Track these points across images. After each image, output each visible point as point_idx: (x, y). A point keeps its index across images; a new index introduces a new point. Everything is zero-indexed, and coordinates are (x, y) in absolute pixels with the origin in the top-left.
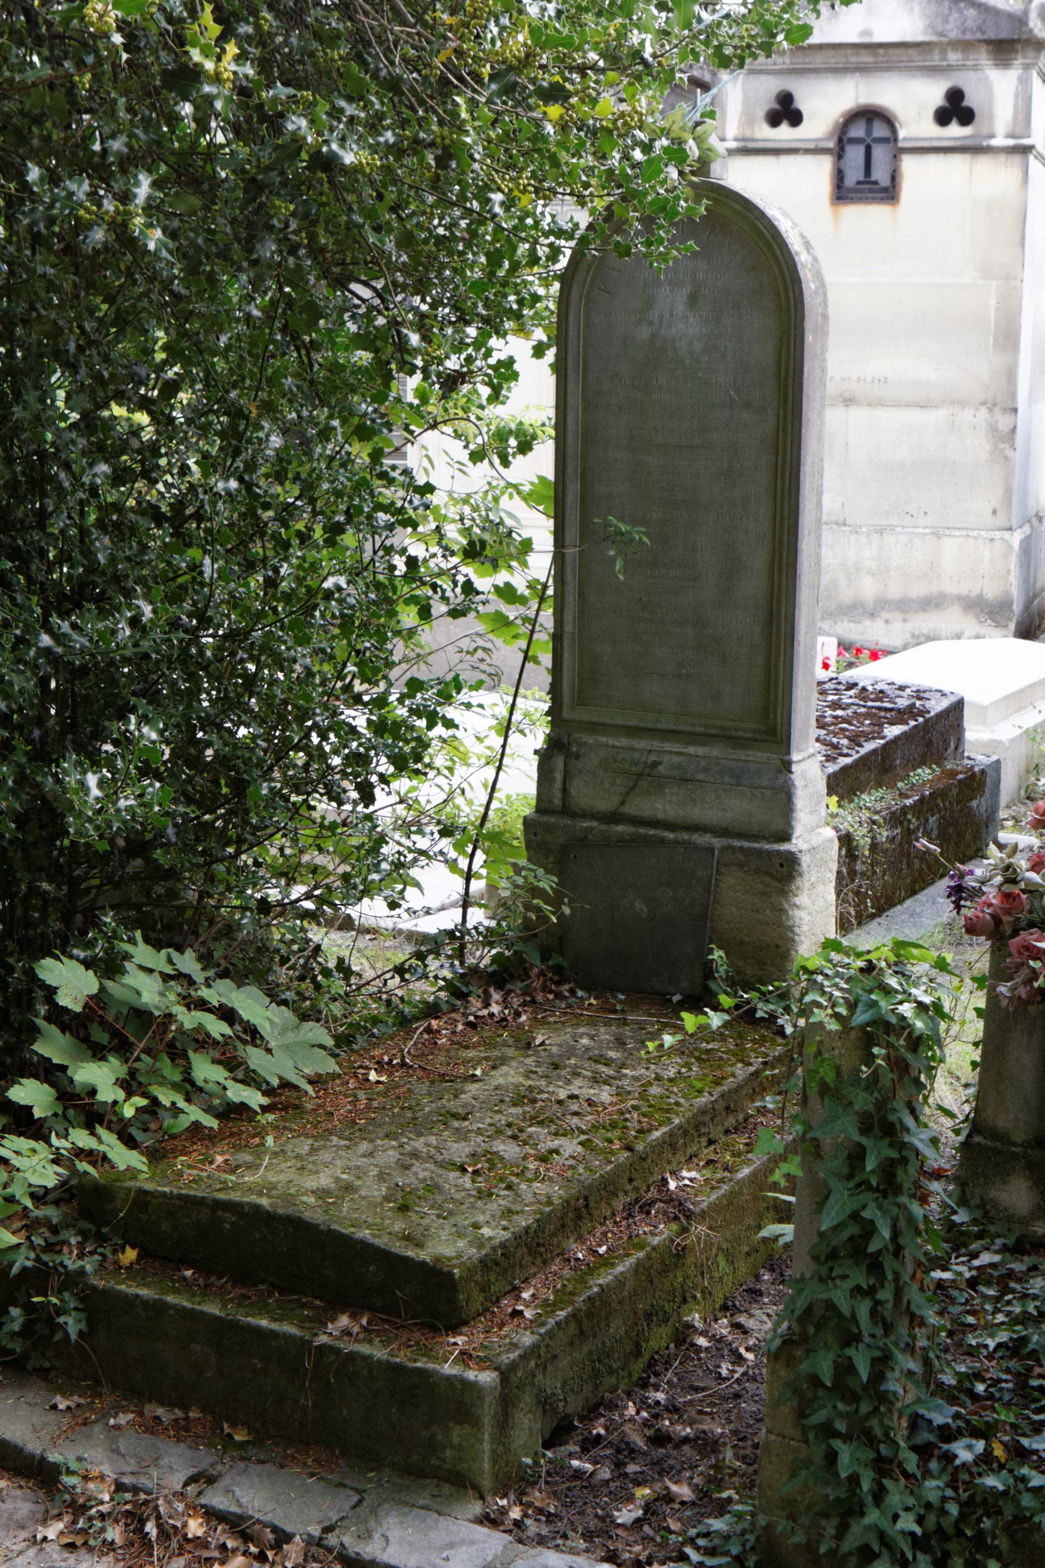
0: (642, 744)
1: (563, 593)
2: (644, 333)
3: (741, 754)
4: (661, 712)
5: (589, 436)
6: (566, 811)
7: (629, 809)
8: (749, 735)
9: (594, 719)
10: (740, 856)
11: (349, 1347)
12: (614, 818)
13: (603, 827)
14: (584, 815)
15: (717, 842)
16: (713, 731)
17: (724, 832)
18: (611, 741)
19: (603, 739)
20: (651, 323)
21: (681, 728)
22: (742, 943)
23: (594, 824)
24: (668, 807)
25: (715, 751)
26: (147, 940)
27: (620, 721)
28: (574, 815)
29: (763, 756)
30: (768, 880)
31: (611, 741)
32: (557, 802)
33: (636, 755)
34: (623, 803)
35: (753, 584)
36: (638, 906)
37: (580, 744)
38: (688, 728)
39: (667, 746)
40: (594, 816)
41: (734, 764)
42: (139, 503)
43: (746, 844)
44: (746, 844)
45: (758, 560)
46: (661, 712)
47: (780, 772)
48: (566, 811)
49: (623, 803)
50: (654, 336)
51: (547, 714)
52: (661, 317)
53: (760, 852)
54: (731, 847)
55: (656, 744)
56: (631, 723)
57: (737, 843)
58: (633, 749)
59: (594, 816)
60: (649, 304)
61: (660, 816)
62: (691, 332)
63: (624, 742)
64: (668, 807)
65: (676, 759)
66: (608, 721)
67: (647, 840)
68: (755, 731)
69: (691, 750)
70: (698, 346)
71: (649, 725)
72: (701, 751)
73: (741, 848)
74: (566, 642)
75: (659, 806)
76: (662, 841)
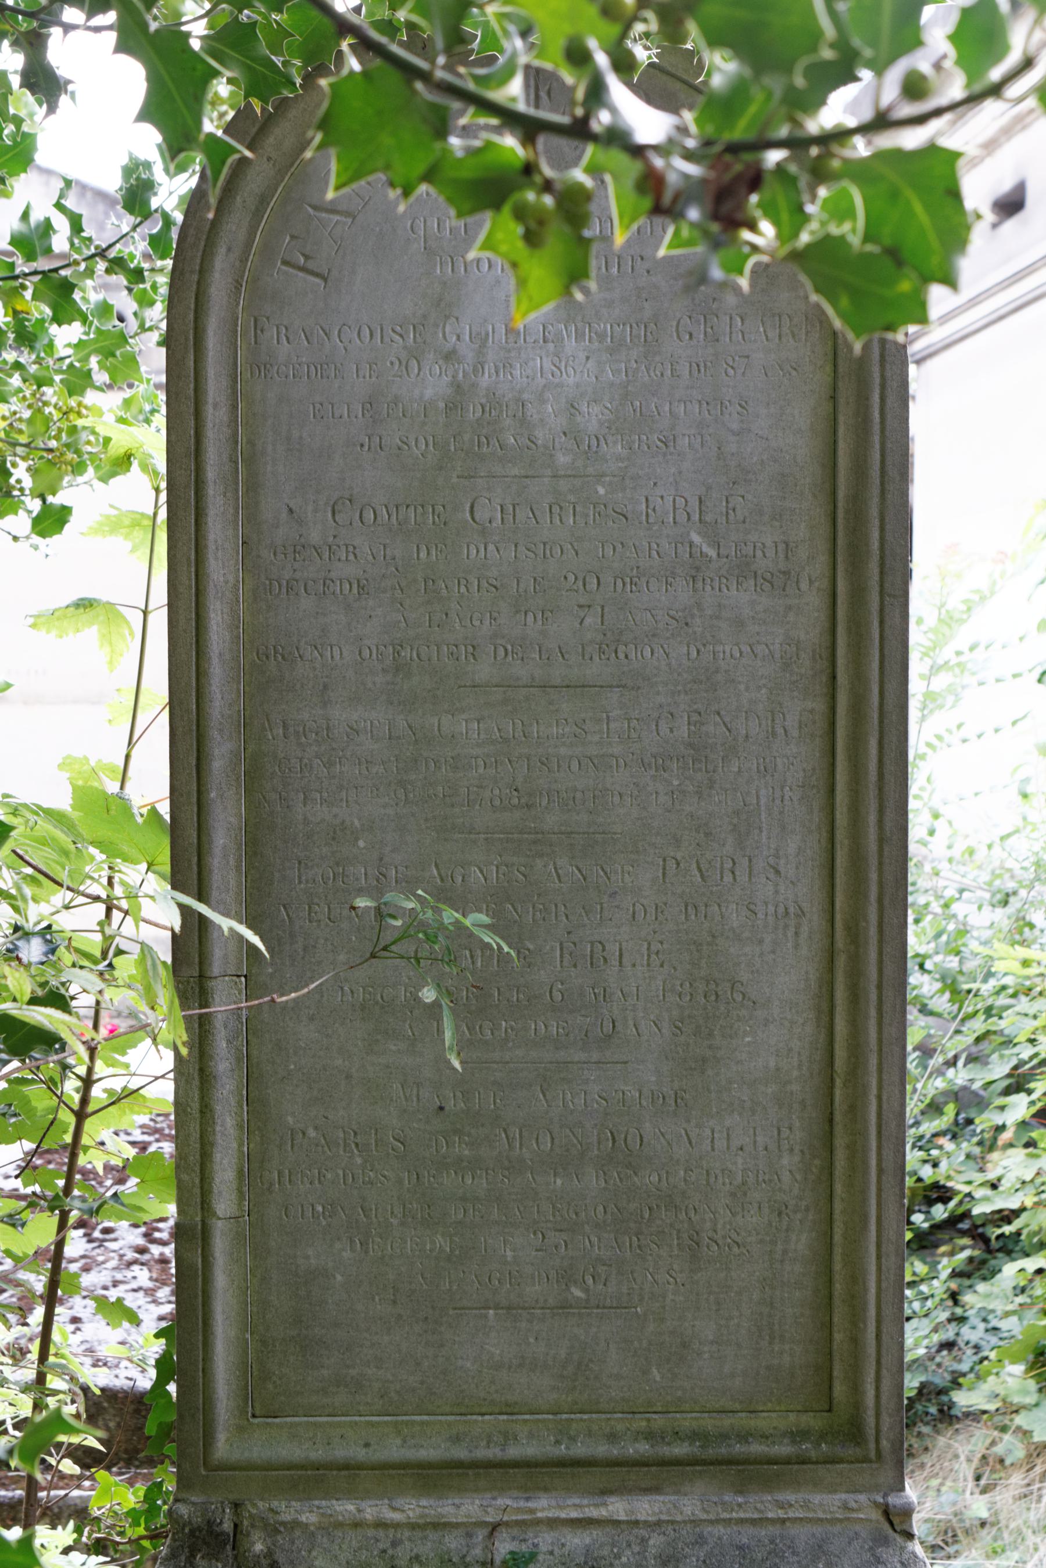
0: (467, 1507)
1: (206, 1109)
2: (432, 384)
3: (764, 1503)
4: (510, 1409)
5: (266, 669)
8: (784, 1449)
9: (318, 1454)
11: (476, 931)
16: (680, 1450)
18: (371, 1510)
19: (346, 1508)
20: (450, 356)
21: (580, 1450)
25: (688, 1504)
26: (134, 1509)
27: (394, 1451)
29: (827, 1502)
31: (371, 1510)
33: (453, 1542)
35: (774, 1039)
37: (273, 1530)
38: (602, 1450)
39: (544, 1506)
41: (745, 1535)
45: (783, 977)
46: (510, 1409)
47: (883, 1541)
50: (455, 404)
52: (481, 340)
55: (505, 1504)
56: (429, 1452)
58: (439, 1526)
60: (444, 304)
62: (571, 380)
63: (411, 1507)
65: (577, 1541)
66: (360, 1454)
68: (798, 1435)
69: (617, 1507)
70: (592, 417)
71: (484, 1453)
72: (645, 1507)
74: (220, 1245)
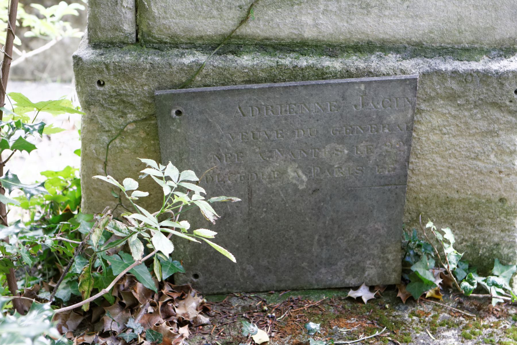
6: (142, 40)
7: (256, 28)
10: (454, 85)
12: (228, 44)
13: (218, 61)
14: (176, 44)
15: (414, 67)
17: (417, 49)
22: (448, 202)
23: (202, 58)
24: (323, 20)
28: (159, 46)
30: (496, 114)
32: (128, 28)
34: (243, 21)
36: (291, 173)
40: (193, 44)
42: (494, 255)
43: (462, 66)
44: (462, 66)
48: (142, 40)
49: (243, 21)
51: (21, 151)
53: (485, 76)
54: (438, 73)
57: (448, 65)
59: (193, 44)
61: (309, 34)
64: (323, 20)
67: (295, 73)
73: (455, 72)
75: (307, 19)
76: (322, 74)
